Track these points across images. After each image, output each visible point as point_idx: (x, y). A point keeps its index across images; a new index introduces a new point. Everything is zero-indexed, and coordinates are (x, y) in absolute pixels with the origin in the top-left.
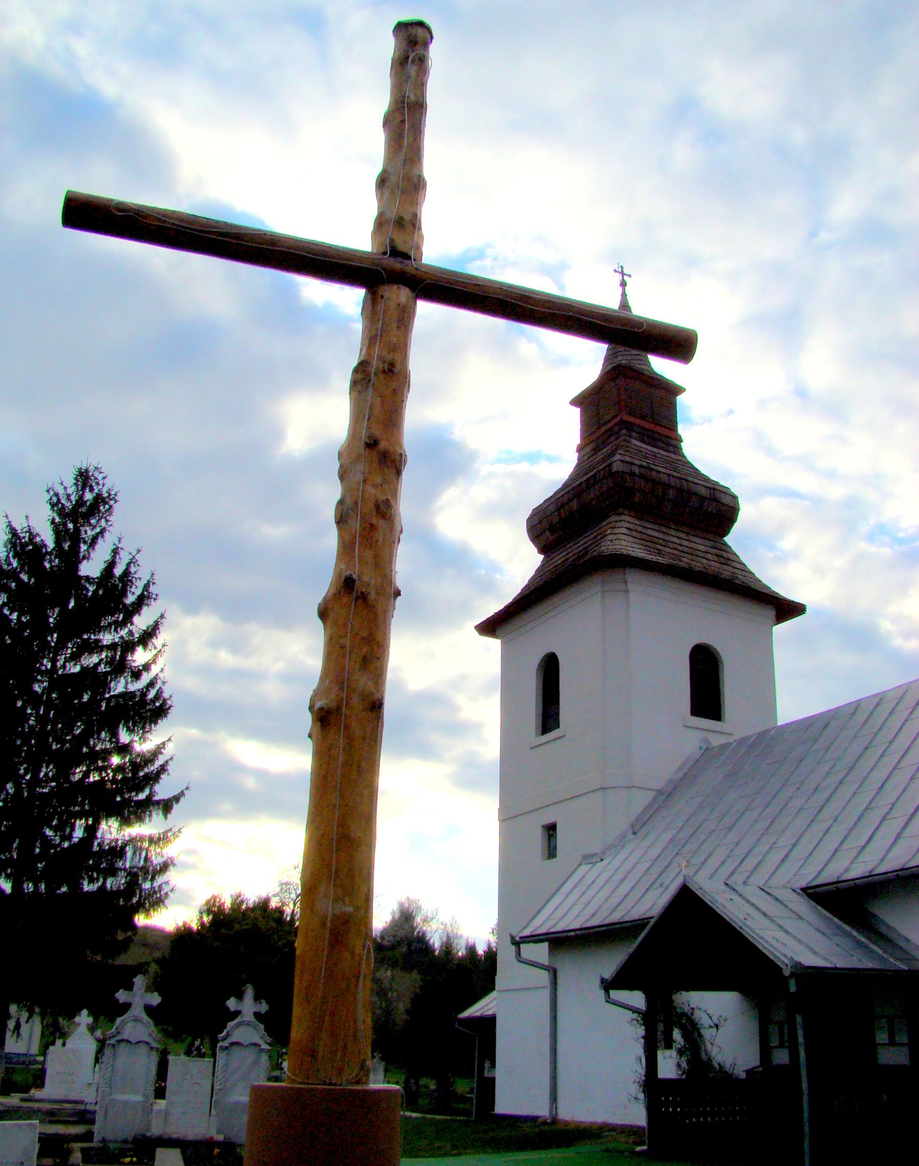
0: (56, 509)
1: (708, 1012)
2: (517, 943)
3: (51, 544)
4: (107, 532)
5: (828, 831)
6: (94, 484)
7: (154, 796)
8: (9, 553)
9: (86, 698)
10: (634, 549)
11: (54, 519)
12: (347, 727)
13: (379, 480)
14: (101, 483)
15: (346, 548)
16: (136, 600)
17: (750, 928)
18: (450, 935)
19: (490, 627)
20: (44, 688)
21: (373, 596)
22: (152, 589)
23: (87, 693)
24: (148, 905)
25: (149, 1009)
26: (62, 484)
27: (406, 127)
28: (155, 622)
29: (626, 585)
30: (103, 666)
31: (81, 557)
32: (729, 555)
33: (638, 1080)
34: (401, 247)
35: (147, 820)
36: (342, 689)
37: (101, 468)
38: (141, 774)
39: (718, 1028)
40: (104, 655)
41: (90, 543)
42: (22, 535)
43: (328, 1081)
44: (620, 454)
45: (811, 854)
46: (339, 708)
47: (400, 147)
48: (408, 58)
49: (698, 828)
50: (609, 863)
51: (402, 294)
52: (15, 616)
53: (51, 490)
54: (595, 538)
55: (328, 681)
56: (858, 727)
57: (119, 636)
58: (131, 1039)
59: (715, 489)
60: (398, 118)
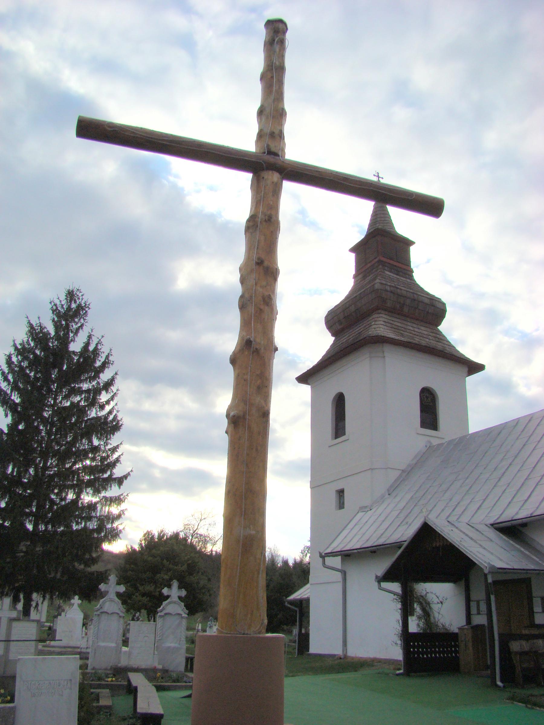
0: (55, 313)
1: (436, 595)
2: (323, 556)
3: (53, 333)
4: (84, 326)
5: (504, 491)
6: (76, 299)
7: (113, 475)
8: (29, 339)
9: (74, 420)
10: (388, 333)
11: (54, 319)
12: (249, 428)
13: (264, 283)
14: (81, 298)
15: (246, 324)
16: (101, 364)
17: (464, 546)
18: (273, 554)
19: (303, 379)
20: (50, 414)
21: (262, 350)
22: (111, 358)
23: (74, 418)
24: (110, 537)
25: (119, 595)
26: (58, 298)
27: (275, 81)
28: (112, 377)
29: (384, 353)
30: (83, 402)
31: (70, 340)
32: (441, 336)
33: (397, 633)
34: (273, 149)
35: (109, 489)
36: (246, 404)
37: (80, 290)
38: (106, 463)
39: (442, 604)
40: (83, 396)
41: (75, 332)
42: (36, 328)
43: (243, 632)
44: (379, 279)
45: (495, 505)
46: (244, 417)
47: (271, 92)
48: (274, 40)
49: (427, 491)
50: (375, 512)
51: (275, 176)
52: (32, 374)
53: (52, 303)
54: (365, 326)
55: (237, 400)
56: (519, 434)
57: (92, 385)
58: (108, 612)
59: (433, 299)
60: (269, 75)
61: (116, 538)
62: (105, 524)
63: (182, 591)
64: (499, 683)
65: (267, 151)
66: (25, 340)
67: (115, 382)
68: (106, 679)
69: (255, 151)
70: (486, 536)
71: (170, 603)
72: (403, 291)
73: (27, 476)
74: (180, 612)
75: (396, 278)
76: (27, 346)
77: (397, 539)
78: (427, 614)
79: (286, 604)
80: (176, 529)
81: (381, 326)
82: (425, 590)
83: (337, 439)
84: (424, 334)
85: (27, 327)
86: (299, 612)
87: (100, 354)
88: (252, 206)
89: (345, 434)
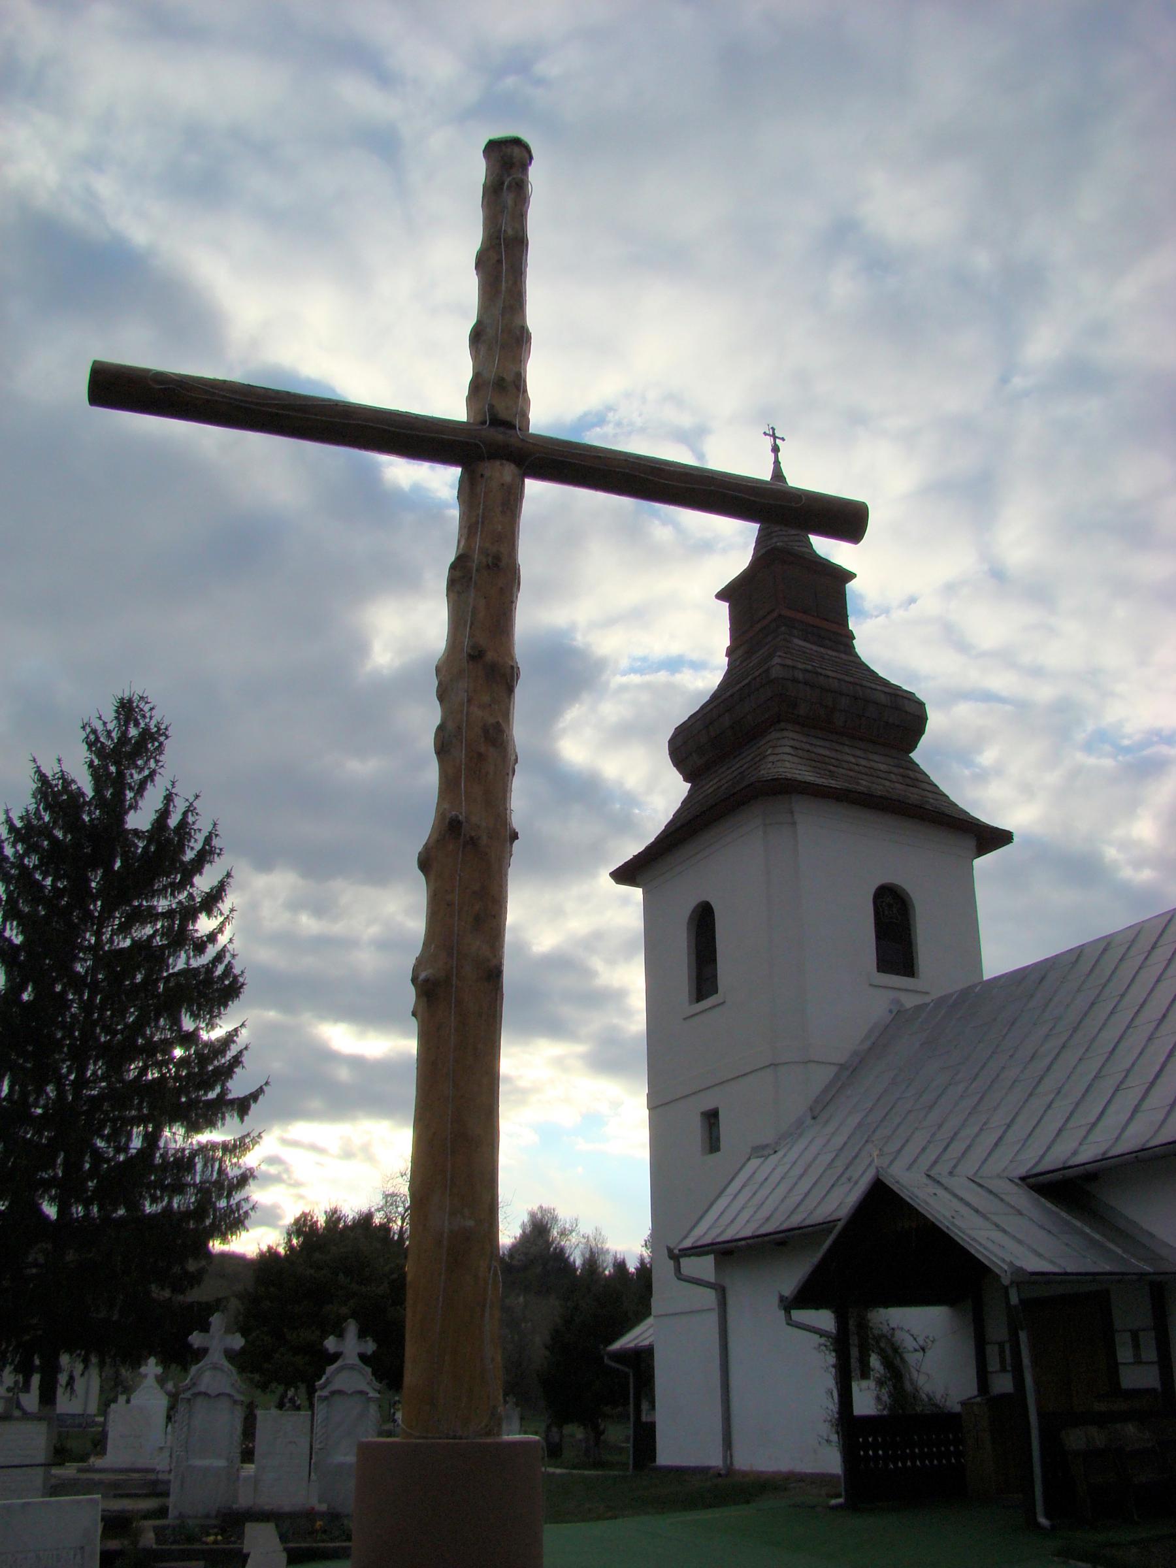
1: (911, 1333)
2: (675, 1256)
3: (89, 792)
4: (157, 775)
5: (1049, 1106)
6: (139, 717)
7: (227, 1094)
8: (39, 805)
11: (92, 762)
13: (486, 699)
14: (148, 715)
16: (196, 856)
17: (959, 1228)
18: (594, 1250)
21: (484, 840)
22: (216, 842)
23: (140, 973)
24: (224, 1227)
26: (100, 718)
29: (793, 816)
31: (127, 807)
33: (829, 1418)
34: (503, 415)
35: (219, 1124)
40: (159, 925)
45: (1030, 1135)
48: (503, 183)
50: (785, 1155)
51: (507, 472)
52: (49, 881)
53: (87, 727)
55: (433, 946)
57: (177, 900)
58: (209, 1392)
59: (896, 695)
61: (239, 1229)
62: (214, 1199)
63: (366, 1342)
64: (1042, 1520)
65: (490, 420)
66: (32, 808)
67: (227, 892)
68: (204, 1539)
69: (465, 420)
70: (1008, 1204)
71: (341, 1369)
72: (831, 680)
73: (42, 1102)
74: (363, 1386)
75: (816, 651)
76: (35, 822)
77: (830, 1215)
78: (895, 1373)
79: (606, 1361)
80: (368, 1206)
81: (786, 757)
82: (886, 1324)
83: (700, 1003)
84: (880, 771)
85: (34, 781)
86: (634, 1376)
87: (193, 834)
88: (461, 536)
89: (716, 992)
